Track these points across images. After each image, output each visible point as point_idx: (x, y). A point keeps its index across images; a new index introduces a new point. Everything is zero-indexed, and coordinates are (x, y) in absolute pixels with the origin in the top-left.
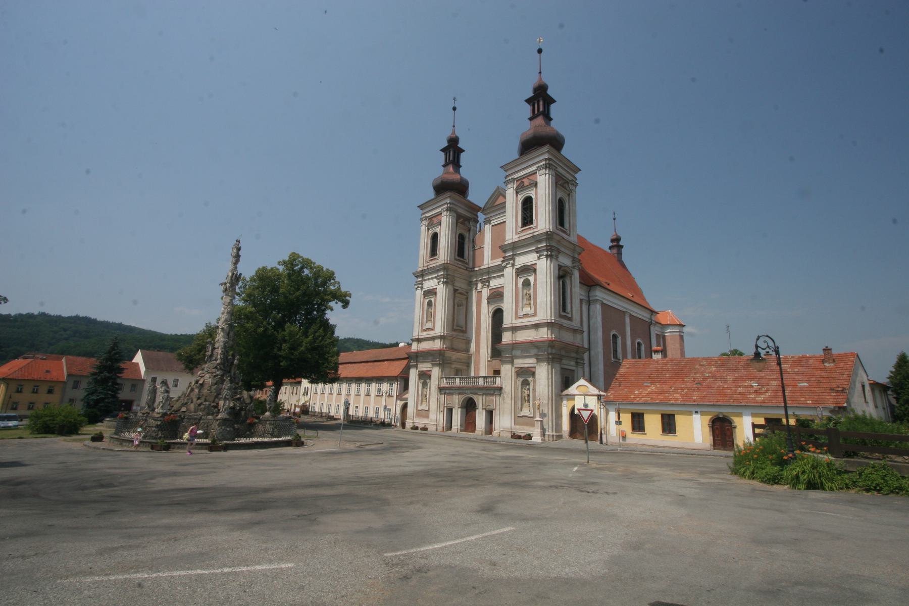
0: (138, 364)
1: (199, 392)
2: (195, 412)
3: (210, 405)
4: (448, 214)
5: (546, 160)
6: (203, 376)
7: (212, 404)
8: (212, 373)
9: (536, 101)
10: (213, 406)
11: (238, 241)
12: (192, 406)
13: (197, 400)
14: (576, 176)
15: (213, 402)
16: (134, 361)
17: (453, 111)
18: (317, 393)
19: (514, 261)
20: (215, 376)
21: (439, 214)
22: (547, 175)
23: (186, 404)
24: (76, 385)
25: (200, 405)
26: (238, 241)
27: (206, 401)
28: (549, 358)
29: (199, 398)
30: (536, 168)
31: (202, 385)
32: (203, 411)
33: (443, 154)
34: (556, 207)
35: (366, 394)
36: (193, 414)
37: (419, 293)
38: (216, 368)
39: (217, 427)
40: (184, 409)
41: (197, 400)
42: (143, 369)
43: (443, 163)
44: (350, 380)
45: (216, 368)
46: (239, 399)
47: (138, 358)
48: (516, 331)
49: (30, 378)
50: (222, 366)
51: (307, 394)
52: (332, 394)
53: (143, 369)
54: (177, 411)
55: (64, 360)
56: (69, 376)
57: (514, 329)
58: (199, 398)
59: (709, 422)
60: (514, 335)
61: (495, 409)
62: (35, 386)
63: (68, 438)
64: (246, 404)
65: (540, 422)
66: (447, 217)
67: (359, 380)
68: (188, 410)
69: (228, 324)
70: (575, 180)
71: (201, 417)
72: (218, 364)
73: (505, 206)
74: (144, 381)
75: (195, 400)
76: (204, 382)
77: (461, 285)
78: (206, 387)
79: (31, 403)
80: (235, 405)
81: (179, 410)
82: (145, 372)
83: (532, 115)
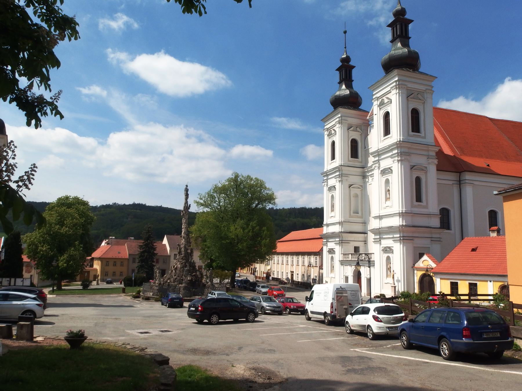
0: (165, 245)
1: (175, 272)
2: (174, 283)
3: (180, 279)
4: (340, 126)
5: (396, 81)
6: (176, 264)
7: (181, 278)
8: (181, 262)
9: (395, 26)
10: (182, 279)
11: (187, 186)
12: (172, 280)
13: (174, 276)
14: (433, 84)
15: (182, 277)
16: (163, 243)
17: (344, 34)
18: (275, 264)
19: (379, 164)
20: (182, 264)
21: (334, 126)
22: (398, 94)
23: (170, 278)
24: (134, 261)
25: (176, 279)
26: (187, 186)
27: (178, 277)
28: (400, 239)
29: (175, 275)
30: (390, 89)
31: (176, 268)
32: (177, 282)
33: (338, 72)
34: (408, 118)
35: (302, 265)
36: (172, 283)
37: (325, 189)
38: (182, 259)
39: (182, 290)
40: (169, 281)
41: (174, 276)
42: (168, 248)
43: (338, 81)
44: (282, 254)
45: (182, 259)
46: (194, 275)
47: (165, 241)
48: (382, 218)
49: (111, 257)
50: (185, 258)
51: (269, 265)
52: (279, 264)
53: (168, 248)
54: (166, 282)
55: (126, 245)
56: (129, 255)
57: (380, 217)
58: (175, 275)
59: (499, 289)
60: (381, 221)
61: (367, 277)
62: (114, 262)
63: (28, 309)
64: (199, 278)
65: (393, 288)
66: (339, 128)
67: (287, 254)
68: (170, 281)
69: (186, 234)
70: (430, 88)
71: (176, 286)
72: (183, 257)
73: (373, 119)
74: (170, 256)
75: (173, 276)
76: (177, 266)
77: (356, 180)
78: (178, 269)
79: (114, 272)
80: (192, 279)
81: (167, 281)
82: (170, 250)
83: (393, 39)
